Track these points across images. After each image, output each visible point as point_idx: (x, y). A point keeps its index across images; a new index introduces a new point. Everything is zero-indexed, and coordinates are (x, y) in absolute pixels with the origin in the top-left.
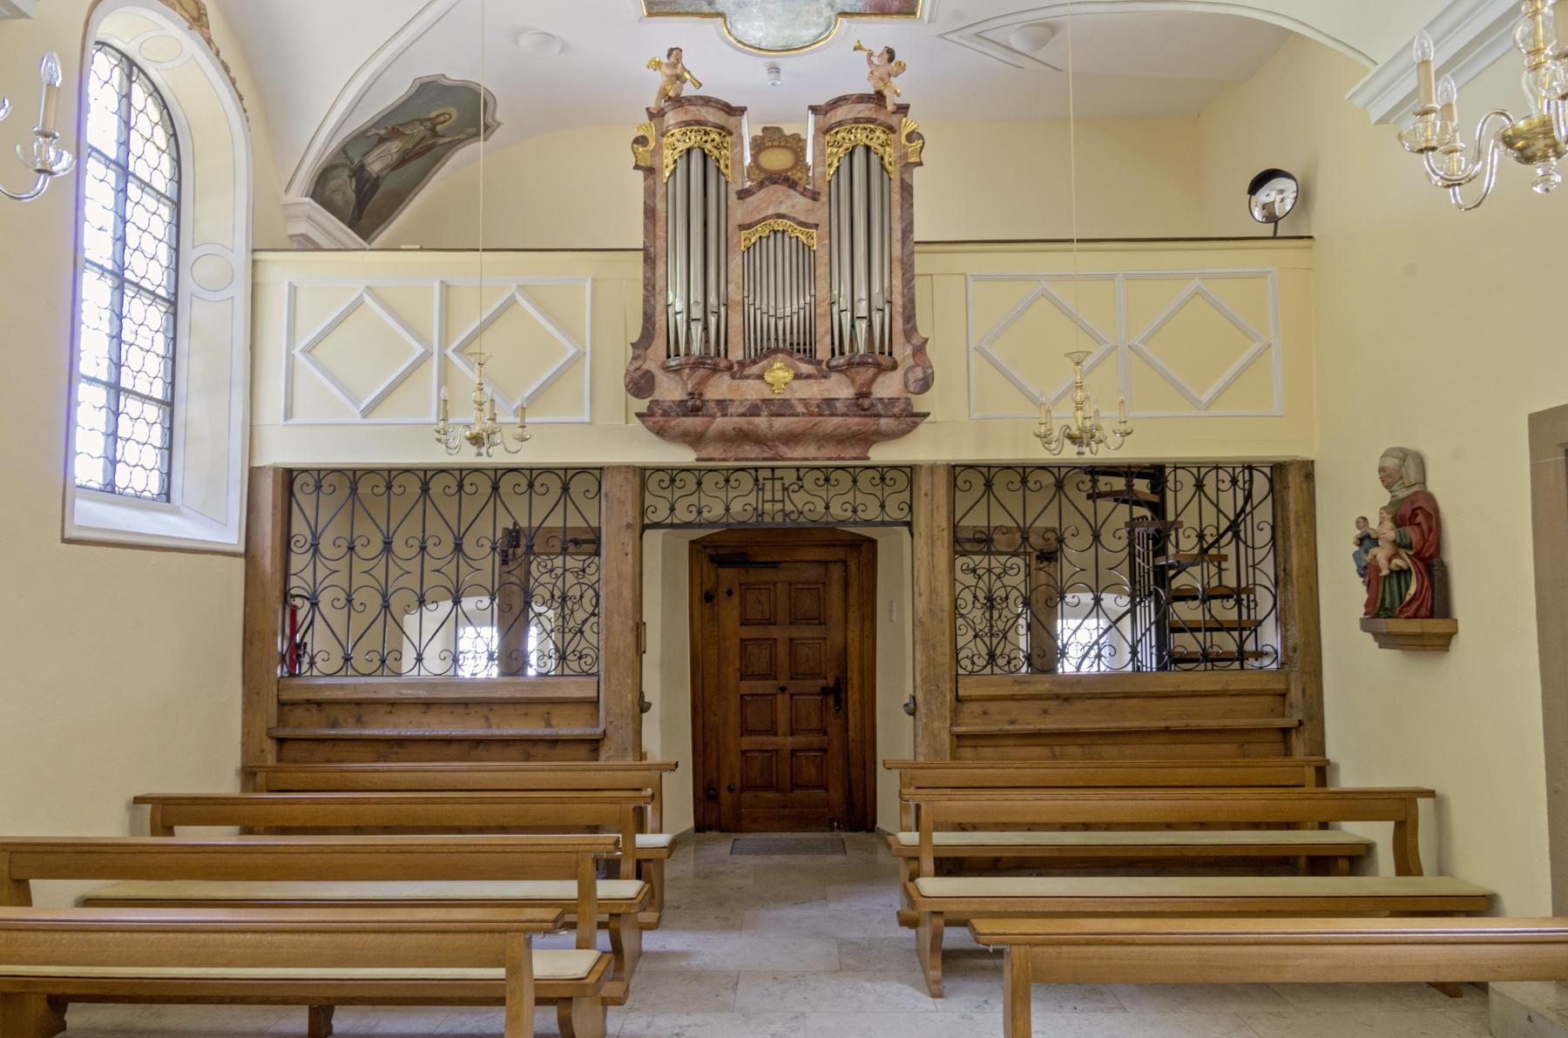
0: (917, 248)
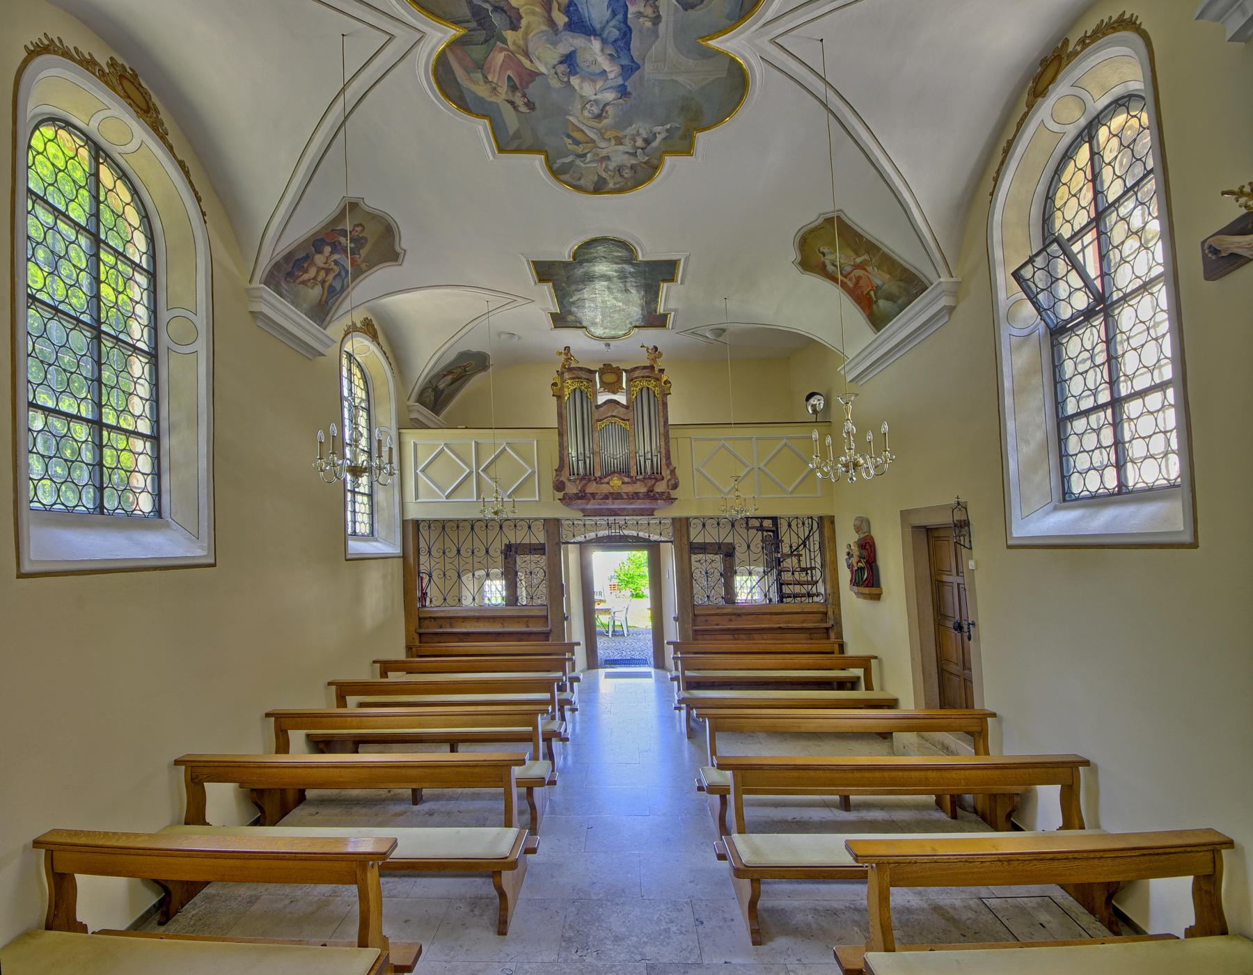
0: (670, 427)
